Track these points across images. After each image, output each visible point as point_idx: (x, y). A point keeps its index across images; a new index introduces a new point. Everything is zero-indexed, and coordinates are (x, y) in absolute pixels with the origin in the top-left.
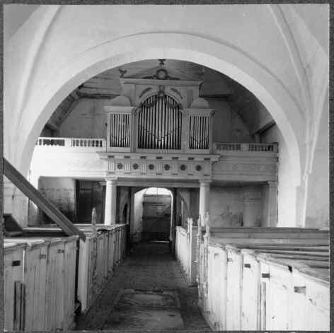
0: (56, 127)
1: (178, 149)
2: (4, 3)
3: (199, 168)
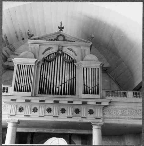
0: (33, 67)
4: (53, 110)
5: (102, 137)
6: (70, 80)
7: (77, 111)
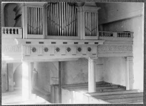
0: (43, 10)
1: (76, 36)
2: (1, 105)
3: (89, 50)
4: (37, 50)
5: (97, 87)
6: (74, 21)
7: (79, 50)
